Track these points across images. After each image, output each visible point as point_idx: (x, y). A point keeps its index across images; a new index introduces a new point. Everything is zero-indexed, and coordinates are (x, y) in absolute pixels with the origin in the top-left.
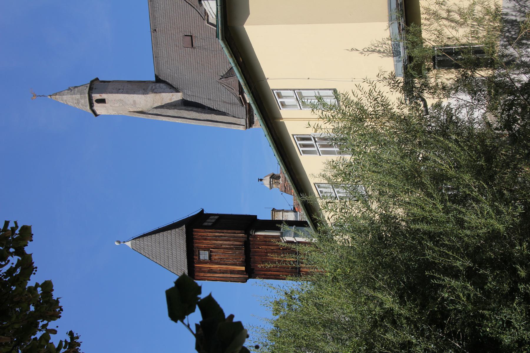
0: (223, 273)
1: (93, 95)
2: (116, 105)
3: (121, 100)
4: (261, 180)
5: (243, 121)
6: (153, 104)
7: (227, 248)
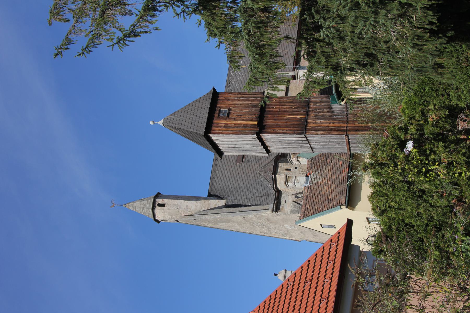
0: (237, 127)
1: (157, 200)
2: (172, 208)
3: (177, 205)
4: (276, 275)
5: (271, 206)
6: (202, 208)
7: (245, 107)
